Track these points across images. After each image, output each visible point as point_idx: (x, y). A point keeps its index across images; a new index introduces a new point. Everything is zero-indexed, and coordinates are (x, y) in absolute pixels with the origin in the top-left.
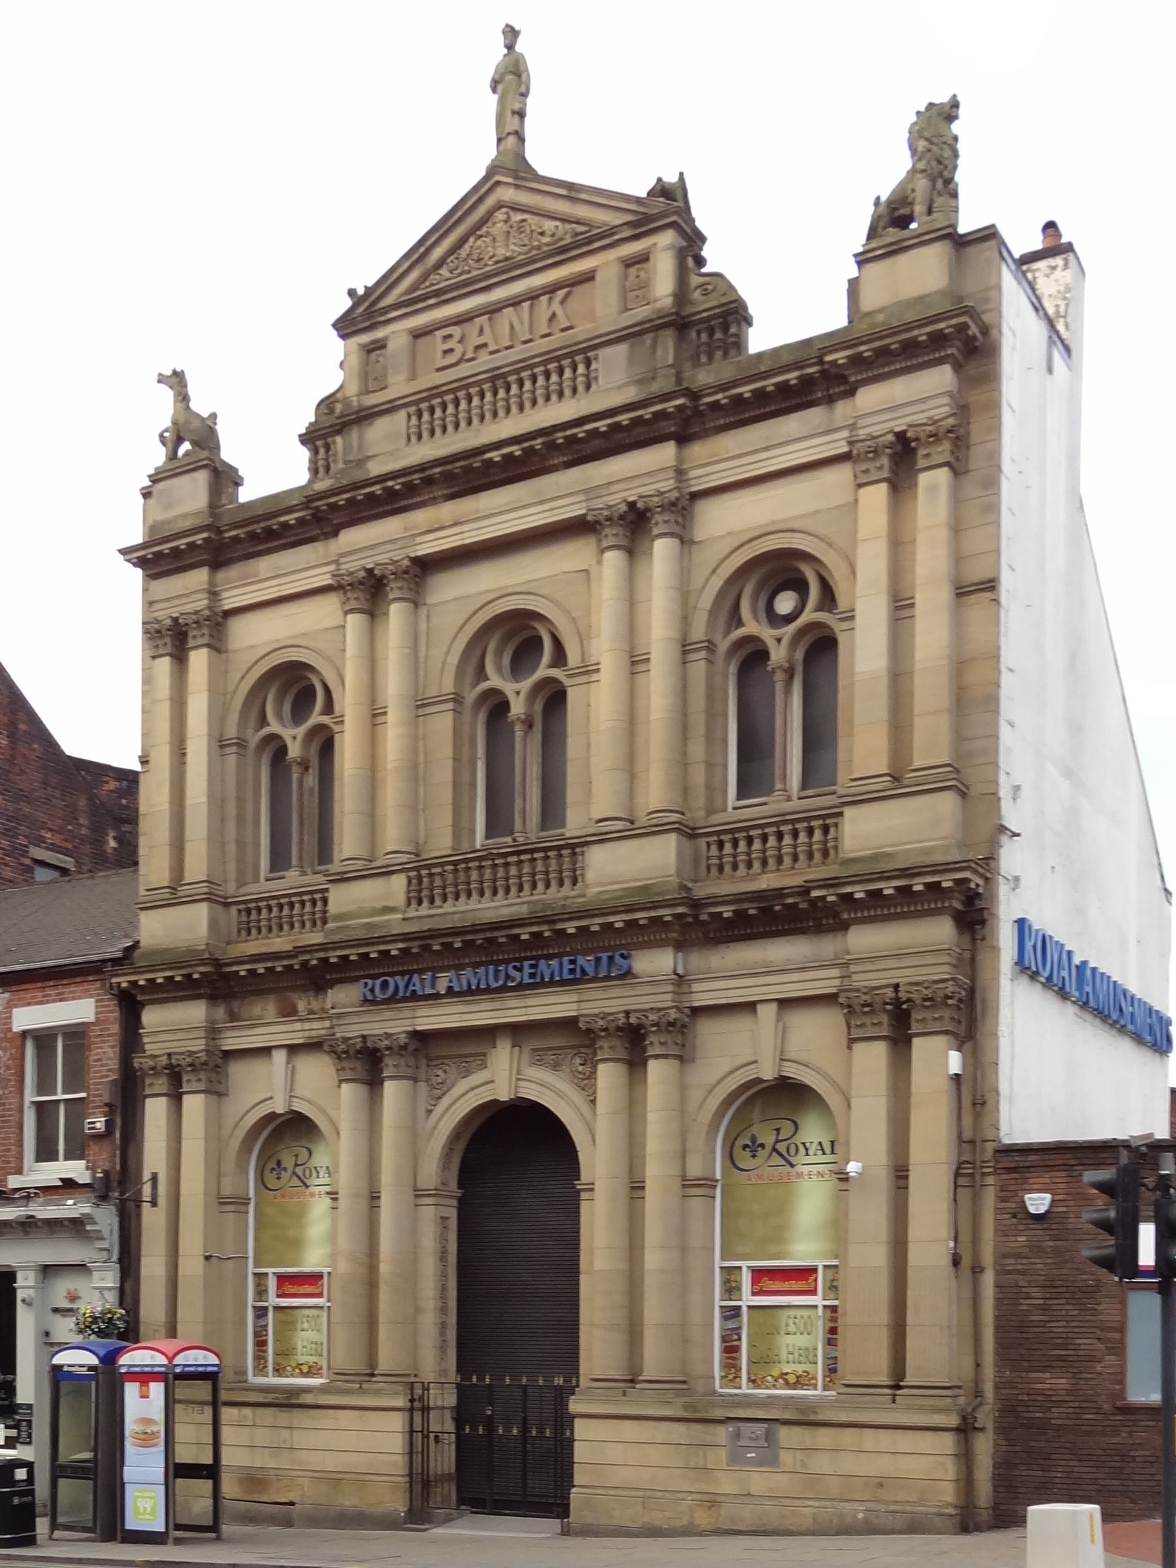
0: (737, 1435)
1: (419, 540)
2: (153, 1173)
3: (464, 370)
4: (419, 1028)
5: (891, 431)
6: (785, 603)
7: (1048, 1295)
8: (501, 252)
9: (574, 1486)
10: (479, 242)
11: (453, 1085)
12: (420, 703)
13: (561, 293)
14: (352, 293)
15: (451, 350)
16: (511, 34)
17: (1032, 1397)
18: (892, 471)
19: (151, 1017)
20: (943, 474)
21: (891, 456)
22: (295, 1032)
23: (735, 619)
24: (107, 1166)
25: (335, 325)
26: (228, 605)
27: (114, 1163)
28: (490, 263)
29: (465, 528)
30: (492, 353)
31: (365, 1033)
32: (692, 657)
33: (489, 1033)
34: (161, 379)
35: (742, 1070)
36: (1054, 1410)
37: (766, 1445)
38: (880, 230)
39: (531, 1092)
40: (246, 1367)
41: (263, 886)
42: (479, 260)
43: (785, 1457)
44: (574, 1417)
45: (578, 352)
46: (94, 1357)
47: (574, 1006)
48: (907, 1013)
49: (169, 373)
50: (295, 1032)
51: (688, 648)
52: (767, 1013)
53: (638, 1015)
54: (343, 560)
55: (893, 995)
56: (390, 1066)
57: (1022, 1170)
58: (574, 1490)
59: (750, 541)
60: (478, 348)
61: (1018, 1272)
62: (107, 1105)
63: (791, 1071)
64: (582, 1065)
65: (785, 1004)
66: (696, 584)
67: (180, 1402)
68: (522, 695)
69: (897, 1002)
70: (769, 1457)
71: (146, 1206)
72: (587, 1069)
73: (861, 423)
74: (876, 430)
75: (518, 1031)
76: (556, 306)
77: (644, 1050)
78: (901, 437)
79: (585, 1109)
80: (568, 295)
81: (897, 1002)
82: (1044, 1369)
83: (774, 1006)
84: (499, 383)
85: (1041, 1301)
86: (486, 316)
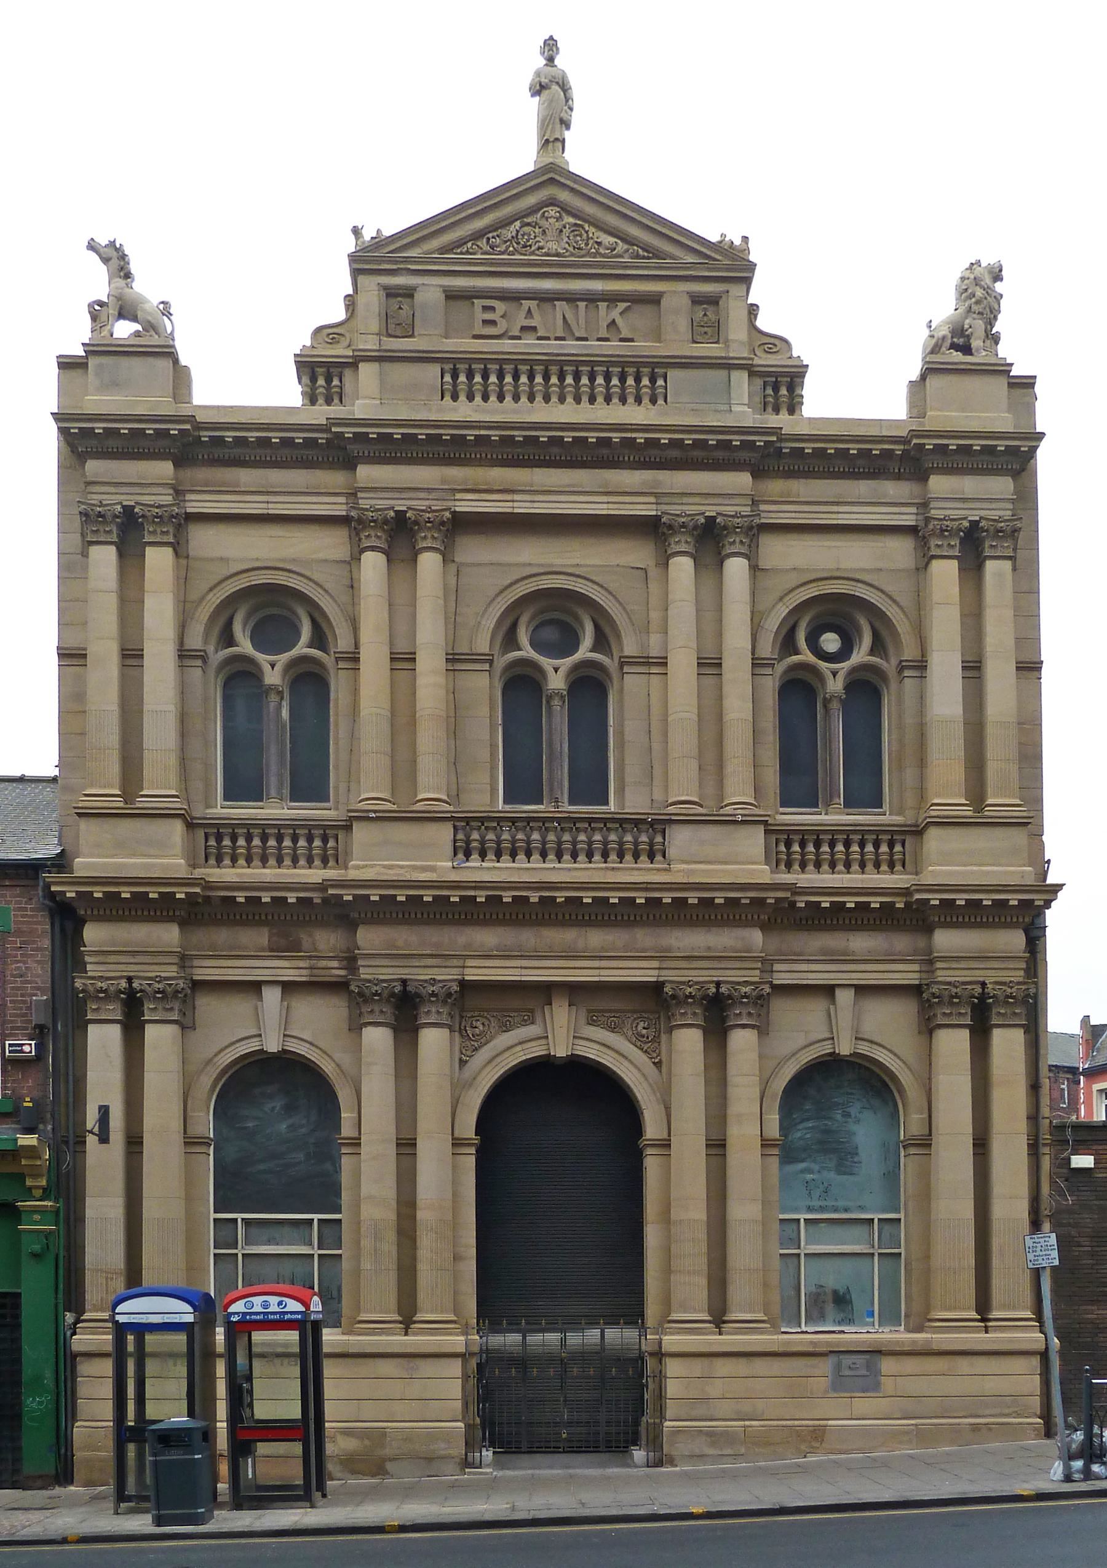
0: (838, 1367)
1: (458, 496)
2: (100, 1107)
3: (507, 345)
4: (467, 978)
5: (121, 503)
6: (831, 642)
7: (1095, 1244)
8: (553, 246)
9: (77, 1421)
10: (526, 229)
11: (492, 1038)
12: (451, 657)
13: (622, 306)
14: (379, 231)
15: (493, 323)
16: (550, 48)
17: (1082, 1325)
18: (118, 536)
19: (93, 934)
20: (435, 558)
21: (118, 526)
22: (289, 970)
23: (510, 641)
24: (36, 1094)
25: (756, 265)
26: (193, 508)
27: (46, 1091)
28: (537, 252)
29: (516, 497)
30: (539, 338)
31: (404, 977)
32: (906, 673)
33: (546, 991)
34: (92, 246)
35: (818, 1045)
36: (1101, 1335)
37: (868, 1373)
38: (943, 349)
39: (591, 1052)
40: (806, 1230)
41: (222, 810)
42: (525, 246)
43: (887, 1384)
44: (75, 1356)
45: (646, 364)
46: (299, 1305)
47: (656, 972)
48: (989, 1007)
49: (103, 241)
50: (289, 970)
51: (184, 653)
52: (272, 996)
53: (728, 986)
54: (360, 495)
55: (714, 990)
56: (430, 1013)
57: (1090, 1143)
58: (78, 1424)
59: (247, 571)
60: (523, 329)
61: (1069, 1225)
62: (37, 1026)
63: (293, 1046)
64: (644, 1028)
65: (861, 990)
66: (194, 595)
67: (154, 1355)
68: (278, 668)
69: (983, 997)
70: (870, 1383)
71: (91, 1140)
72: (651, 1033)
73: (360, 495)
74: (107, 499)
75: (575, 991)
76: (615, 314)
77: (416, 1018)
78: (128, 510)
79: (651, 1070)
80: (627, 309)
81: (983, 997)
82: (1092, 1302)
83: (851, 992)
84: (554, 369)
85: (1090, 1249)
86: (536, 302)
